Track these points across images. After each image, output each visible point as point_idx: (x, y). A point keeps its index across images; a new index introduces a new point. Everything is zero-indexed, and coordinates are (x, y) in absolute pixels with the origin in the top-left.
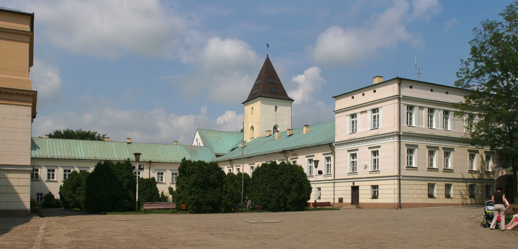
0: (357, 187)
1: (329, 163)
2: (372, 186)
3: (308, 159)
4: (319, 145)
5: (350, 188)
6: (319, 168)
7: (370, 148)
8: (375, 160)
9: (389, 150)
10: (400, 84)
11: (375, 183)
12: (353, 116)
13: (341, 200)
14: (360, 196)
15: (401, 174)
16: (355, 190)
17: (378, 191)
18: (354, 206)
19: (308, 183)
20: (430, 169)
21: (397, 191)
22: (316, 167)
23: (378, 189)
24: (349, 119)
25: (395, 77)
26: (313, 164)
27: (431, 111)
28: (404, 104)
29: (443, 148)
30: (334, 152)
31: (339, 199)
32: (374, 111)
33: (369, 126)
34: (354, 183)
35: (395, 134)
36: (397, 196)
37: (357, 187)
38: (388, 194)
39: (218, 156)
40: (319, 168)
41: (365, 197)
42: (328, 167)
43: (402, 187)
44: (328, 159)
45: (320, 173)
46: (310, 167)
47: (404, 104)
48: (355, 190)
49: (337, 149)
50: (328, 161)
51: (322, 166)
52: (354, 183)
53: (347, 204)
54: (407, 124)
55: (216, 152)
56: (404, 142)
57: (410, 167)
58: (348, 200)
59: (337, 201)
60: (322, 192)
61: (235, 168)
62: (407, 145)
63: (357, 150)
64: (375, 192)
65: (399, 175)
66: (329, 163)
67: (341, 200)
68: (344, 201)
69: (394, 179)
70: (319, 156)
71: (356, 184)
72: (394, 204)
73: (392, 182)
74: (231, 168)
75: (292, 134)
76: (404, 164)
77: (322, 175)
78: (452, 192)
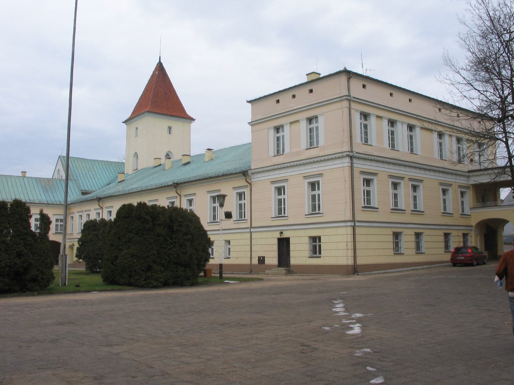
0: (287, 240)
1: (242, 202)
2: (310, 237)
3: (211, 197)
4: (227, 175)
5: (276, 242)
6: (227, 208)
7: (305, 177)
8: (313, 197)
9: (336, 181)
10: (349, 79)
11: (315, 233)
12: (278, 129)
13: (261, 260)
14: (292, 254)
15: (357, 219)
16: (284, 244)
17: (320, 246)
18: (283, 270)
19: (203, 233)
20: (396, 209)
21: (351, 245)
22: (222, 205)
23: (320, 241)
24: (272, 133)
25: (342, 69)
26: (217, 204)
27: (392, 123)
28: (357, 111)
29: (410, 179)
30: (250, 184)
31: (259, 258)
32: (310, 120)
33: (304, 143)
34: (281, 233)
35: (345, 154)
36: (351, 253)
37: (287, 240)
38: (336, 251)
39: (84, 193)
40: (227, 208)
41: (299, 254)
42: (310, 132)
43: (358, 238)
44: (241, 196)
45: (228, 215)
46: (214, 208)
47: (357, 111)
48: (284, 244)
49: (255, 179)
50: (240, 199)
51: (231, 204)
52: (281, 233)
53: (270, 267)
54: (362, 141)
55: (83, 189)
56: (360, 165)
57: (368, 206)
58: (272, 259)
59: (255, 261)
60: (230, 246)
61: (105, 211)
62: (362, 173)
63: (286, 180)
64: (315, 247)
65: (354, 221)
66: (242, 202)
67: (261, 260)
68: (267, 262)
69: (346, 226)
70: (228, 189)
71: (286, 235)
72: (347, 266)
73: (343, 231)
74: (100, 211)
75: (189, 163)
76: (360, 201)
77: (231, 220)
78: (424, 245)
